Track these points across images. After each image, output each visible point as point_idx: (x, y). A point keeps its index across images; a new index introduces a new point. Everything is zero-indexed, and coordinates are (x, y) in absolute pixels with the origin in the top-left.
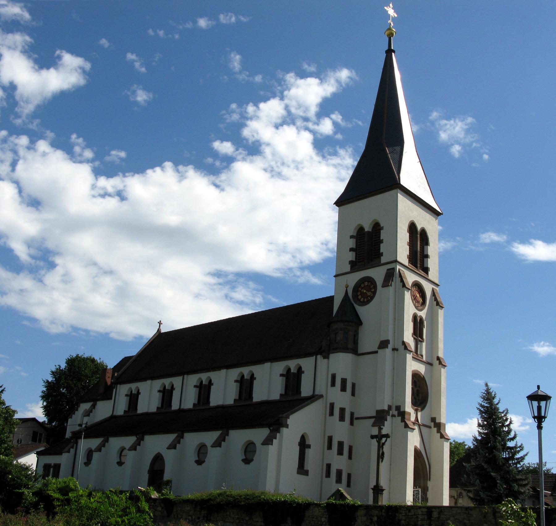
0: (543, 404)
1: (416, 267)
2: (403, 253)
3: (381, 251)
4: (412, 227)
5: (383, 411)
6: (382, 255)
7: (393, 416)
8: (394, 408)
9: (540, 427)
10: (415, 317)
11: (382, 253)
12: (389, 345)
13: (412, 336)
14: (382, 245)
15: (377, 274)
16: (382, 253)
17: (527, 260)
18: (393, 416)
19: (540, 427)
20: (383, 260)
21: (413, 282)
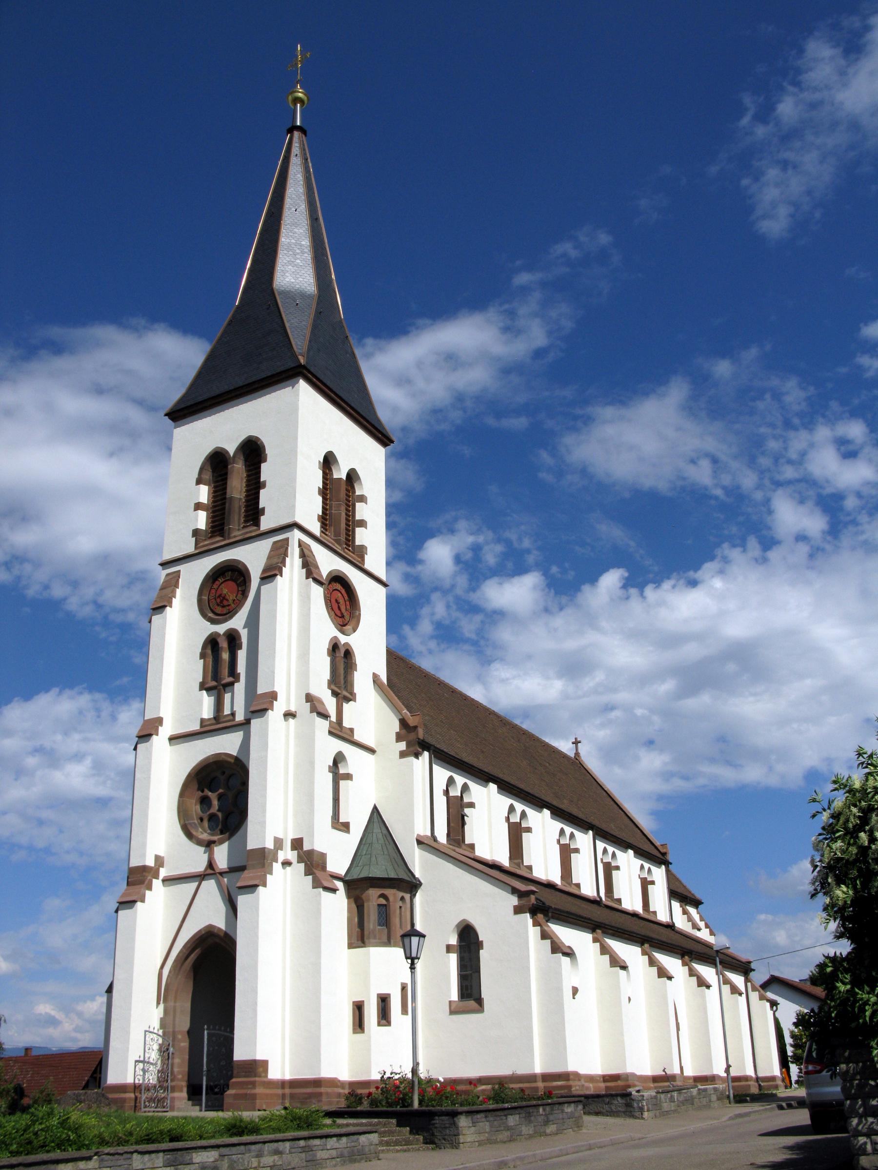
0: (422, 939)
1: (338, 542)
2: (308, 509)
3: (261, 506)
4: (300, 541)
5: (144, 869)
6: (263, 514)
7: (286, 864)
8: (288, 845)
9: (412, 967)
10: (334, 647)
11: (264, 509)
12: (361, 511)
13: (329, 687)
14: (263, 493)
15: (252, 556)
16: (264, 509)
17: (769, 528)
18: (286, 864)
19: (412, 967)
20: (266, 523)
21: (330, 573)
